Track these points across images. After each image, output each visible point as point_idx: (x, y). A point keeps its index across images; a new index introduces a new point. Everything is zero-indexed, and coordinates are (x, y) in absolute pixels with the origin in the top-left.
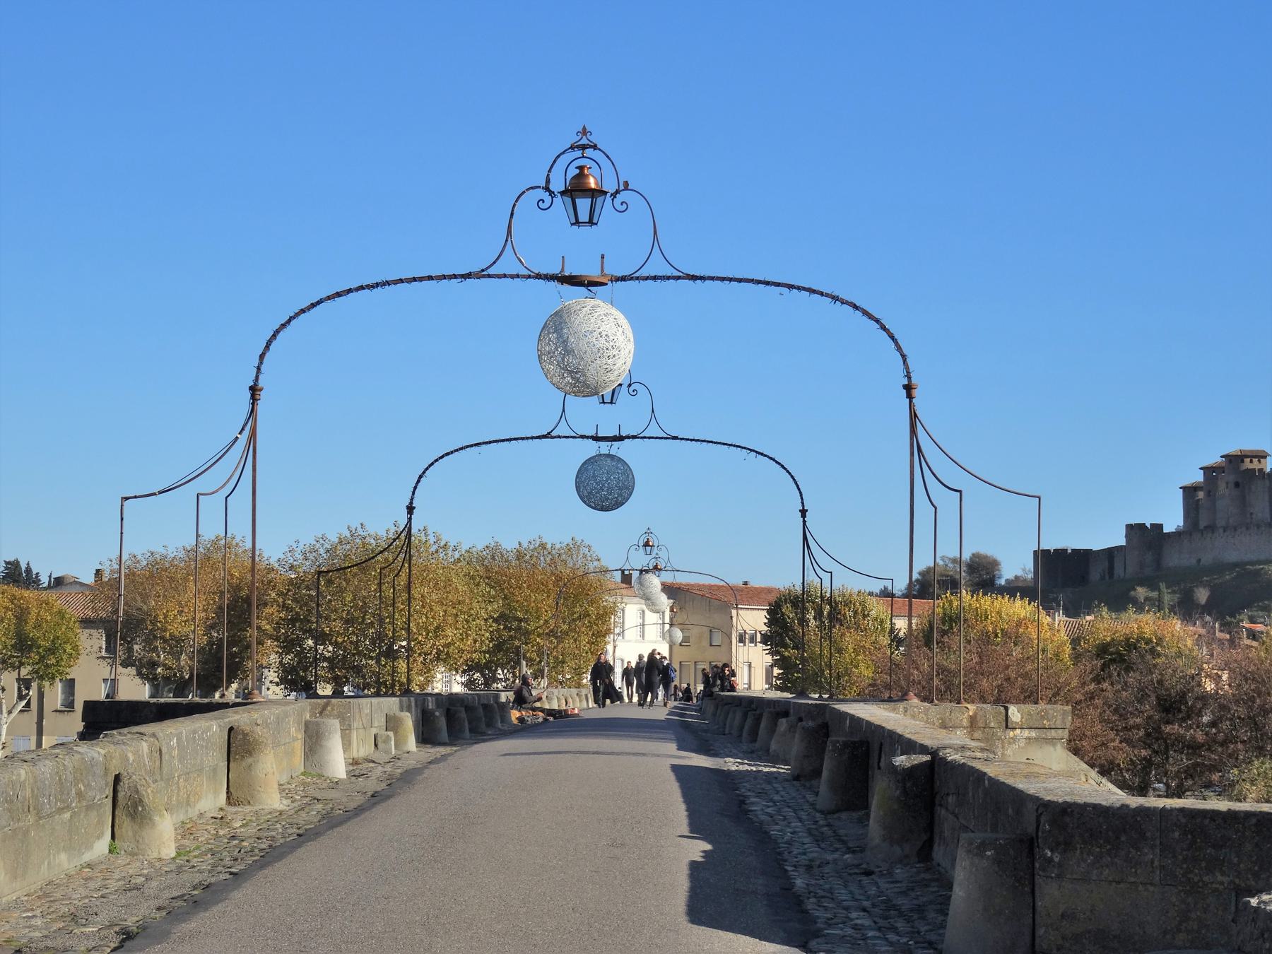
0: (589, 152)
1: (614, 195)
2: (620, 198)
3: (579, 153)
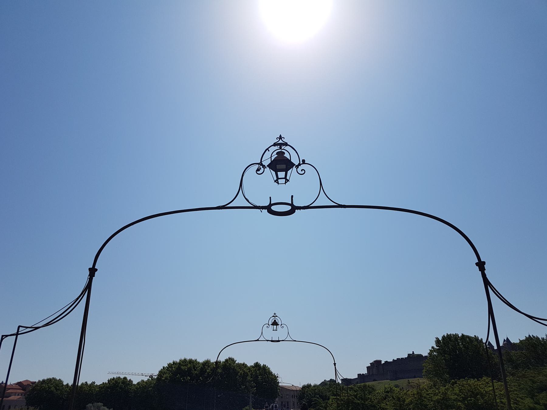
1: (297, 167)
2: (300, 168)
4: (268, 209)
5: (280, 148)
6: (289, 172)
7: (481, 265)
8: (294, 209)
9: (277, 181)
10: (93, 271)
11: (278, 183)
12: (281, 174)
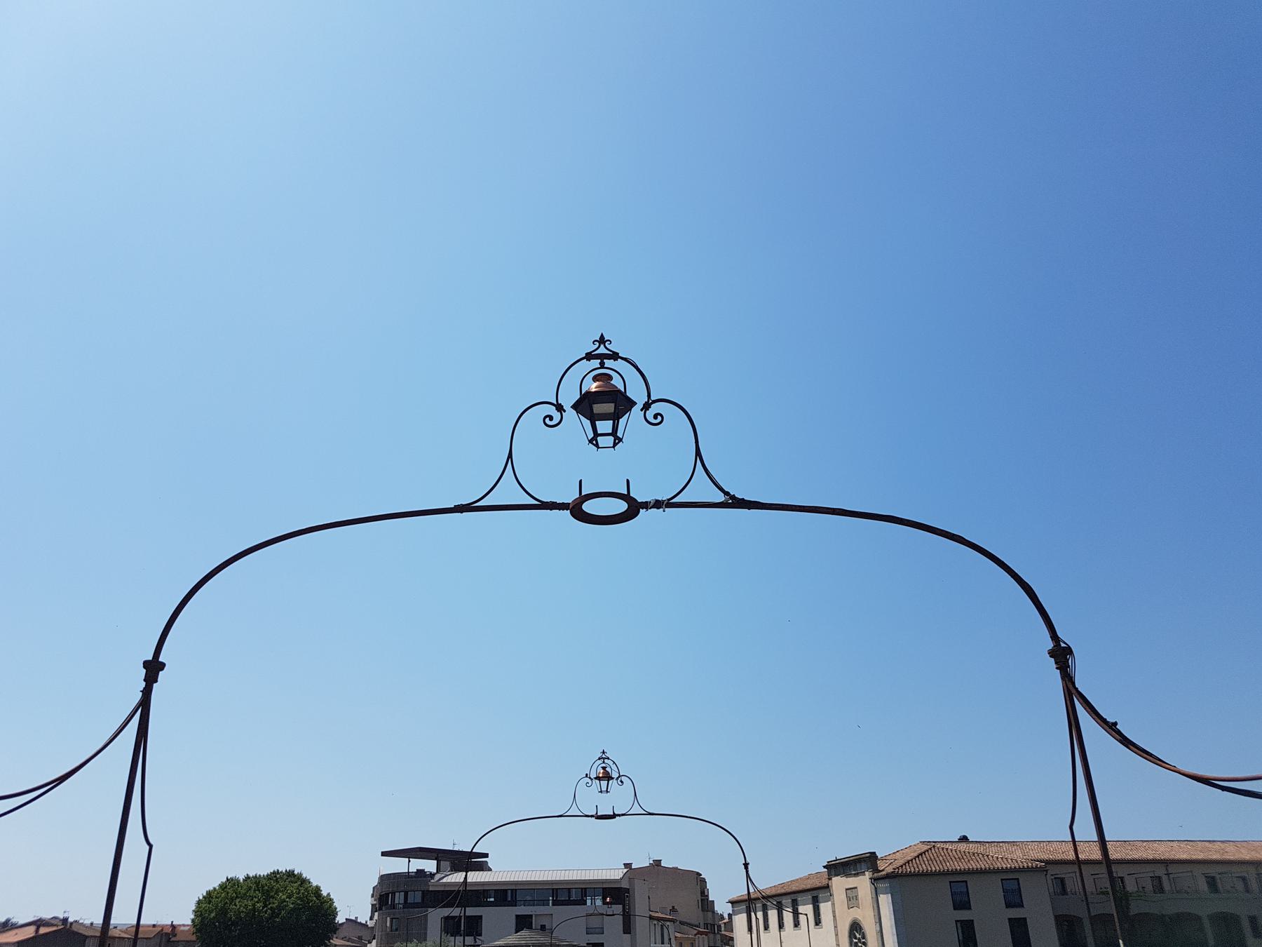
0: (608, 363)
1: (646, 407)
3: (596, 363)
4: (577, 512)
5: (602, 366)
6: (622, 421)
7: (1062, 655)
8: (634, 508)
9: (593, 441)
10: (153, 668)
11: (597, 445)
12: (605, 426)
